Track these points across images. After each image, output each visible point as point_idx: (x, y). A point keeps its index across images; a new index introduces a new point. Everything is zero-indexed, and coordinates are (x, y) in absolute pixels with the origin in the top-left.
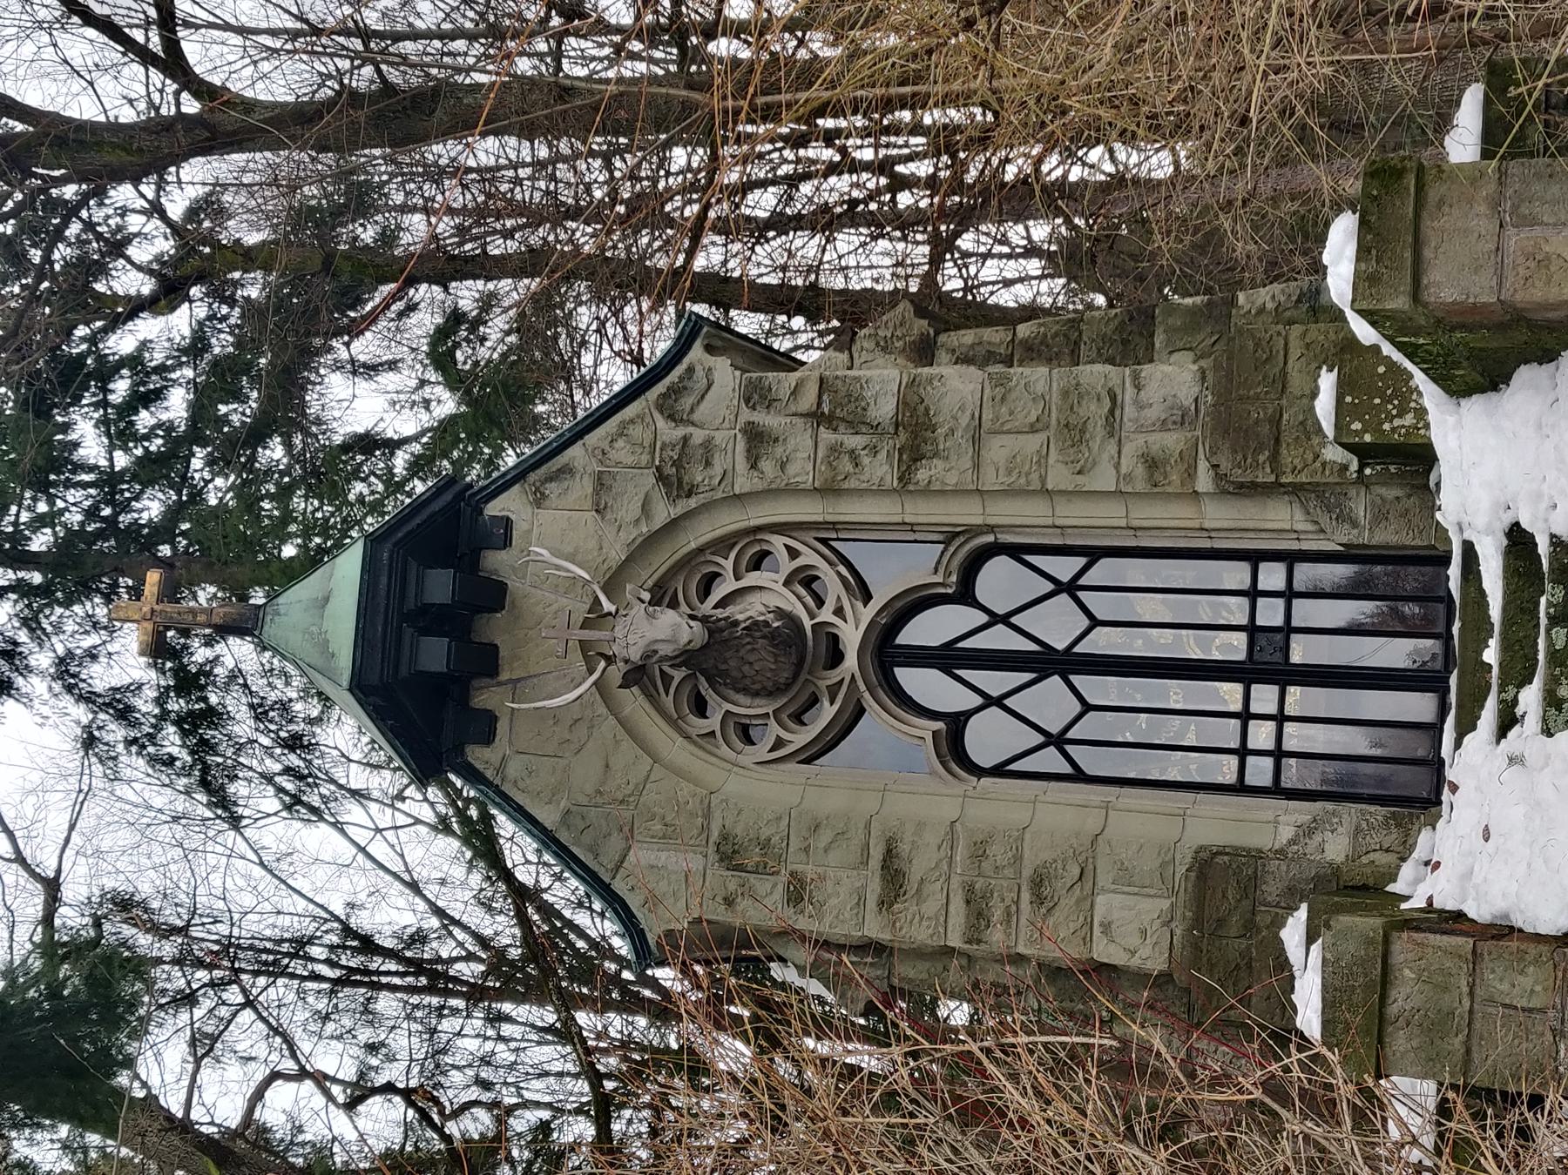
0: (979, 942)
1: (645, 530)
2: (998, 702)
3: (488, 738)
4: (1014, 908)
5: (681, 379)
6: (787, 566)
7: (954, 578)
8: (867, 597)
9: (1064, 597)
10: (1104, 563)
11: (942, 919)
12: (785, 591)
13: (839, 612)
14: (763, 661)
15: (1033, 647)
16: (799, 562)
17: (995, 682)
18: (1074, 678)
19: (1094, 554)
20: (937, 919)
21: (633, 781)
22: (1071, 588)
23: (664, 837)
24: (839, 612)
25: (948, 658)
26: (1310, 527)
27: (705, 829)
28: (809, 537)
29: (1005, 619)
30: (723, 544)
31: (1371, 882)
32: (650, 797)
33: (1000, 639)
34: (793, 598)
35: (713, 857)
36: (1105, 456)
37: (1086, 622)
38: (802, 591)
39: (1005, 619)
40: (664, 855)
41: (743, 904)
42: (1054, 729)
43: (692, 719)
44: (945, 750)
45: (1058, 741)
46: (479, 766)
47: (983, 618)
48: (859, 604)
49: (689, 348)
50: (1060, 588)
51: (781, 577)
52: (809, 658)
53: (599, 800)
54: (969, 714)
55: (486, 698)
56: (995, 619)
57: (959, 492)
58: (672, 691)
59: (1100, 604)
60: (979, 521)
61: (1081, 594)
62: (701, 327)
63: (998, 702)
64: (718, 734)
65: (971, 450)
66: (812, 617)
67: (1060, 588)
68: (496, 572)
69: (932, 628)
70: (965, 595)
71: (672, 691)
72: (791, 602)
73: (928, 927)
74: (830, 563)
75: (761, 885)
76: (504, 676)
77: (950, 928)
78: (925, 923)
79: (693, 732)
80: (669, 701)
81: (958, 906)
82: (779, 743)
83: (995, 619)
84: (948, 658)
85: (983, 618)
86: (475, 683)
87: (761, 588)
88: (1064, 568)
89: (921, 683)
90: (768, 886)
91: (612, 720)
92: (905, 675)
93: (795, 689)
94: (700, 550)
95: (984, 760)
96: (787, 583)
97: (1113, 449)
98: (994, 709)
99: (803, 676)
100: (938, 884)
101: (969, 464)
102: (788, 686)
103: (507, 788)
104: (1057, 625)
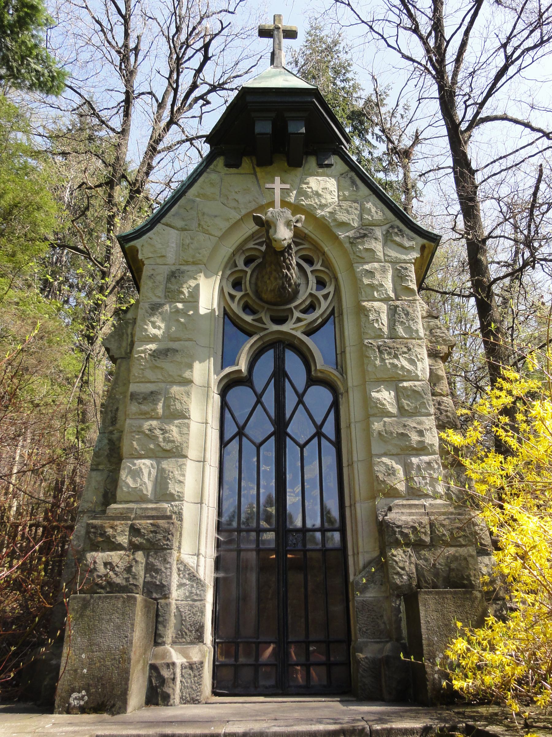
0: (131, 399)
1: (332, 224)
2: (259, 401)
3: (228, 165)
4: (148, 416)
5: (407, 235)
6: (319, 294)
7: (319, 374)
8: (309, 333)
9: (314, 430)
10: (333, 450)
11: (143, 380)
12: (307, 294)
13: (299, 320)
14: (270, 285)
15: (288, 416)
16: (322, 299)
17: (269, 399)
18: (273, 438)
19: (337, 444)
20: (143, 377)
21: (209, 228)
22: (319, 434)
23: (183, 245)
24: (299, 320)
25: (280, 375)
26: (361, 564)
27: (187, 263)
28: (335, 304)
29: (301, 401)
30: (327, 263)
31: (161, 619)
32: (201, 237)
33: (291, 400)
34: (304, 298)
35: (173, 268)
36: (390, 447)
37: (302, 441)
38: (307, 303)
39: (301, 401)
40: (174, 245)
41: (150, 283)
42: (247, 431)
43: (243, 258)
44: (232, 376)
45: (241, 433)
46: (215, 163)
47: (301, 390)
48: (302, 329)
49: (423, 238)
50: (319, 428)
51: (314, 292)
52: (275, 308)
53: (200, 215)
54: (252, 387)
55: (246, 163)
56: (300, 397)
57: (363, 373)
58: (256, 247)
59: (311, 449)
60: (350, 384)
61: (316, 439)
62: (434, 242)
63: (259, 401)
64: (237, 269)
65: (386, 377)
66: (296, 307)
67: (319, 428)
68: (306, 162)
69: (293, 365)
70: (312, 381)
71: (256, 247)
72: (302, 297)
73: (139, 374)
74: (322, 315)
75: (160, 292)
76: (258, 169)
77: (138, 384)
78: (140, 372)
79: (237, 258)
80: (251, 245)
81: (151, 387)
82: (232, 297)
83: (300, 397)
84: (280, 375)
85: (301, 390)
86: (254, 158)
87: (308, 283)
88: (329, 429)
89: (267, 363)
90: (160, 294)
91: (238, 217)
92: (270, 354)
93: (257, 301)
94: (324, 253)
95: (229, 398)
96: (311, 295)
97: (395, 451)
98: (255, 399)
99: (266, 306)
100: (160, 377)
101: (379, 376)
102: (261, 299)
103: (205, 175)
104: (299, 428)
